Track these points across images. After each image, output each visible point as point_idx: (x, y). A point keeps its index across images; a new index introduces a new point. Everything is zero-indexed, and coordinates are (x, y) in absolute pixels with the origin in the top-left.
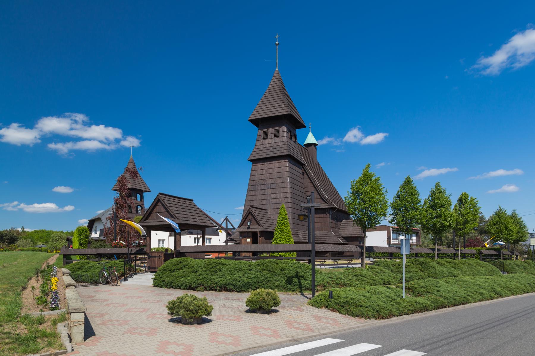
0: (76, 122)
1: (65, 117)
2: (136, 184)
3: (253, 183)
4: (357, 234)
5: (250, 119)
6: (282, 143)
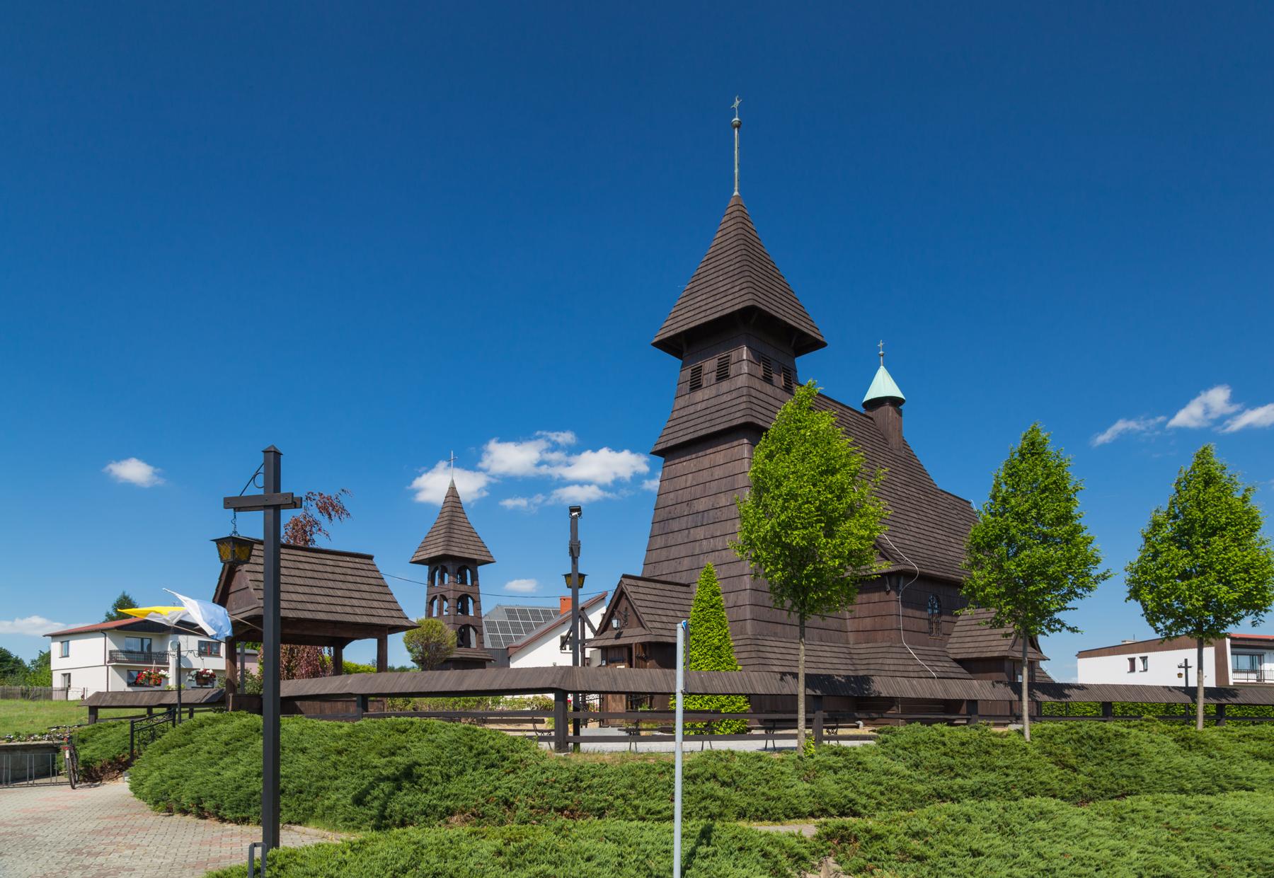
0: (555, 447)
1: (536, 438)
2: (457, 544)
3: (663, 514)
4: (1000, 648)
5: (656, 340)
6: (734, 395)
